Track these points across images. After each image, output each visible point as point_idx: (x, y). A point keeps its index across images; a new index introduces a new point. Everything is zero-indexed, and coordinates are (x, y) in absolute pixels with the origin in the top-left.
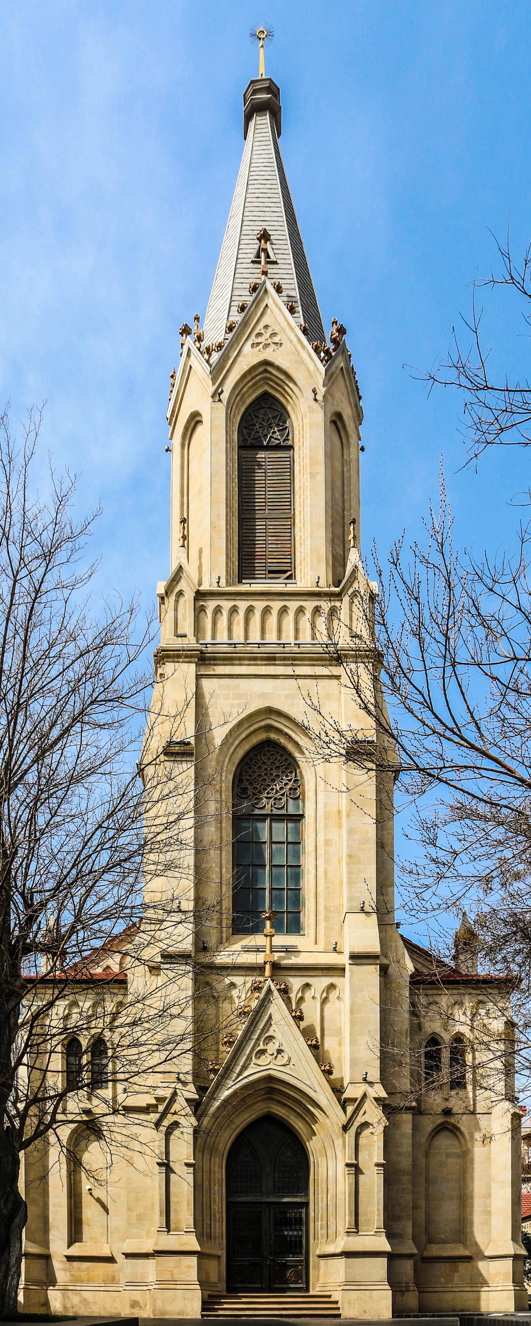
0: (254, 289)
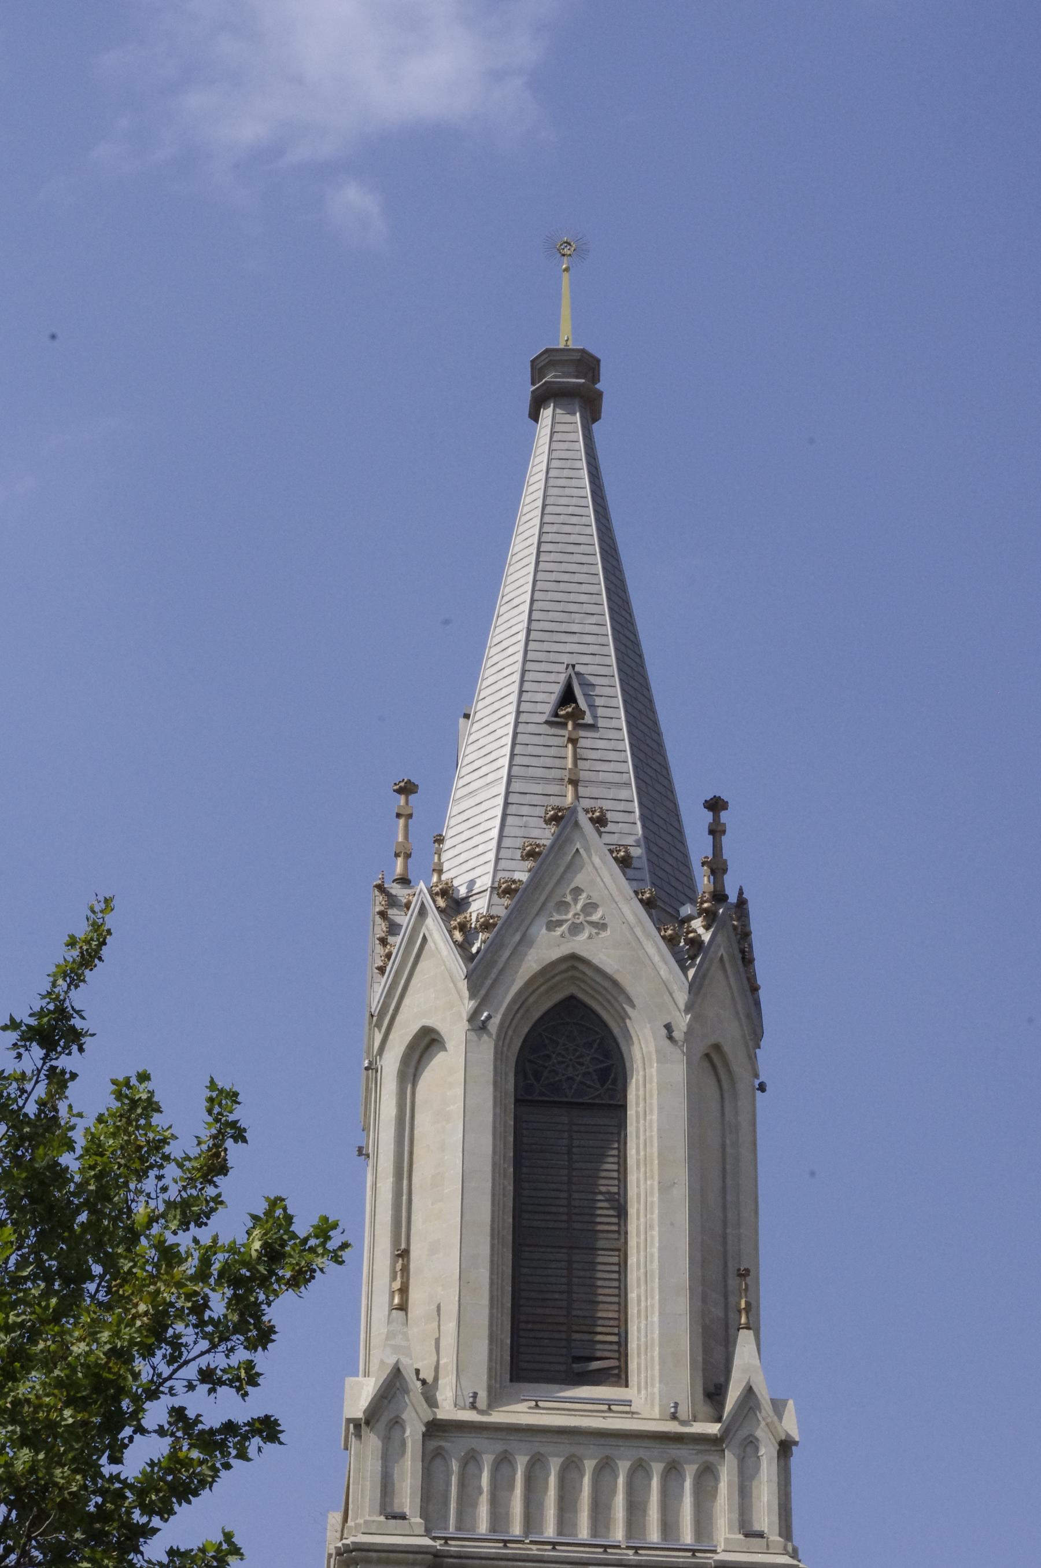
0: (556, 819)
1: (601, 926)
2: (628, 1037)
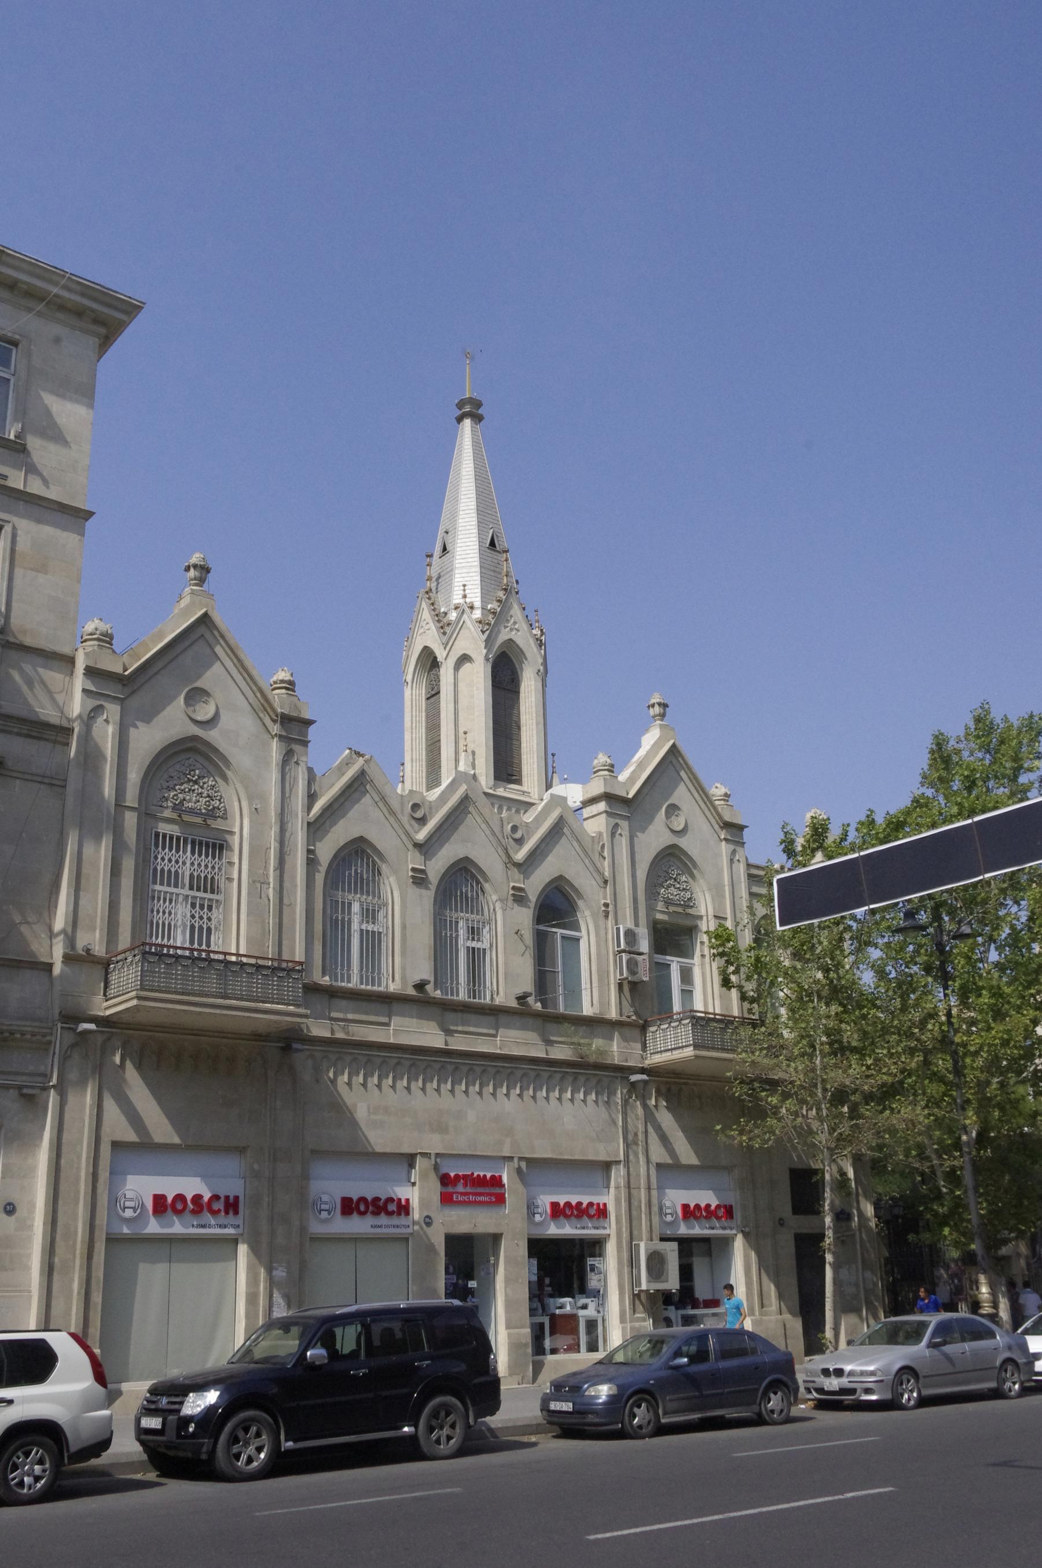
1: (518, 630)
2: (522, 669)
